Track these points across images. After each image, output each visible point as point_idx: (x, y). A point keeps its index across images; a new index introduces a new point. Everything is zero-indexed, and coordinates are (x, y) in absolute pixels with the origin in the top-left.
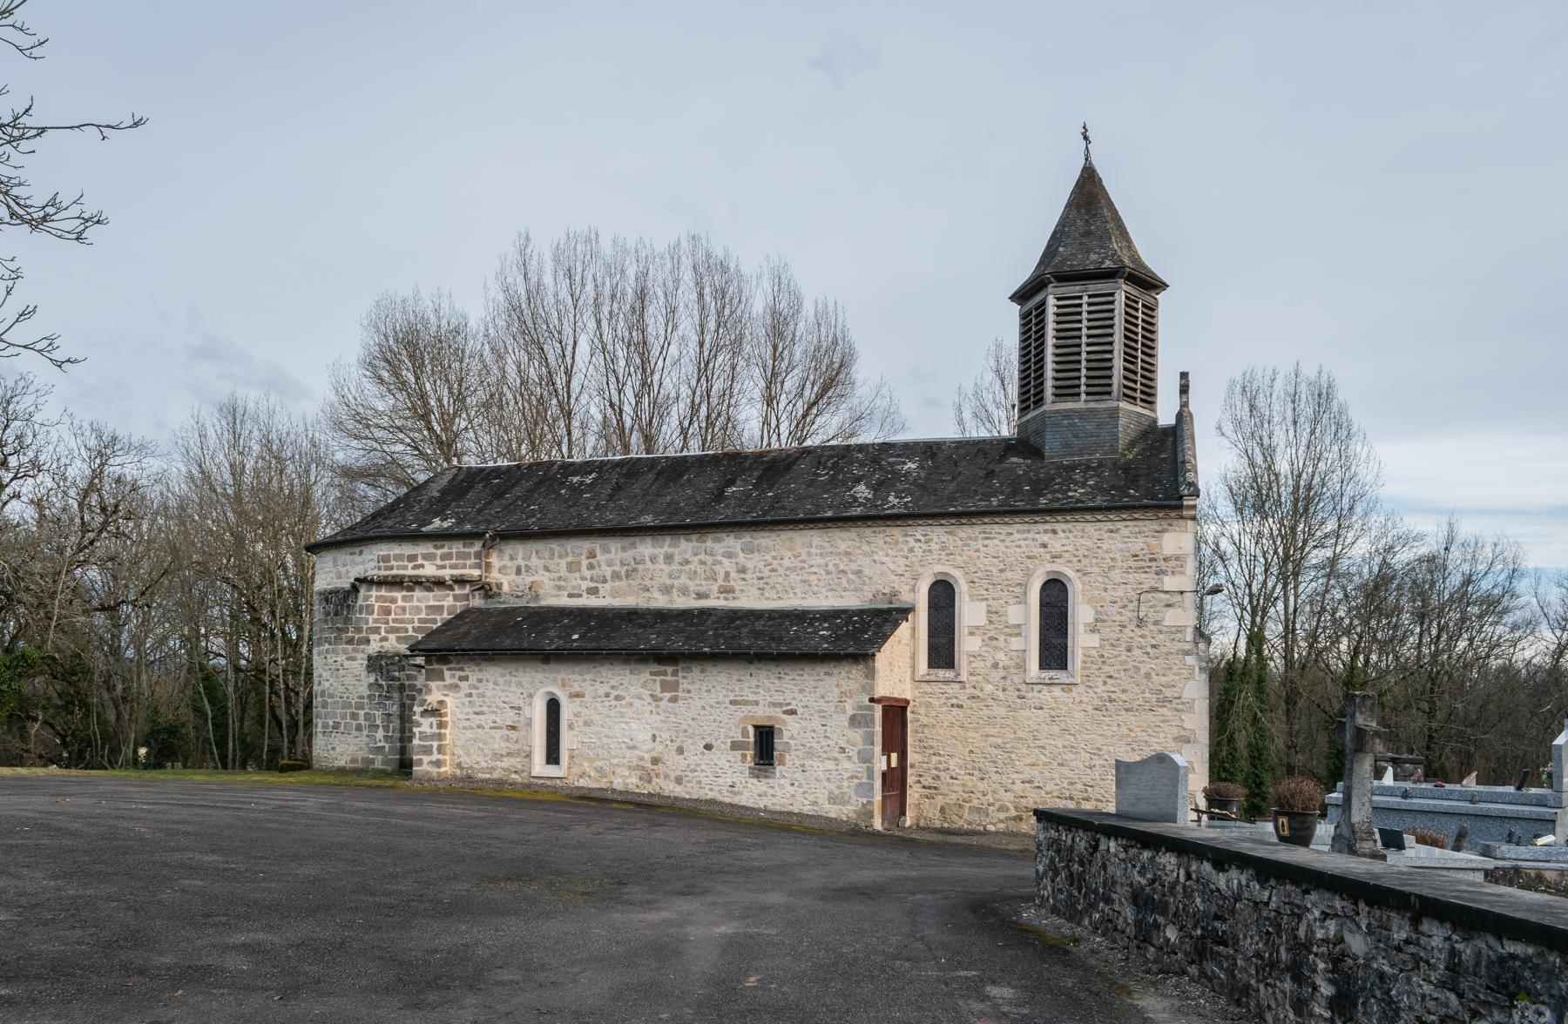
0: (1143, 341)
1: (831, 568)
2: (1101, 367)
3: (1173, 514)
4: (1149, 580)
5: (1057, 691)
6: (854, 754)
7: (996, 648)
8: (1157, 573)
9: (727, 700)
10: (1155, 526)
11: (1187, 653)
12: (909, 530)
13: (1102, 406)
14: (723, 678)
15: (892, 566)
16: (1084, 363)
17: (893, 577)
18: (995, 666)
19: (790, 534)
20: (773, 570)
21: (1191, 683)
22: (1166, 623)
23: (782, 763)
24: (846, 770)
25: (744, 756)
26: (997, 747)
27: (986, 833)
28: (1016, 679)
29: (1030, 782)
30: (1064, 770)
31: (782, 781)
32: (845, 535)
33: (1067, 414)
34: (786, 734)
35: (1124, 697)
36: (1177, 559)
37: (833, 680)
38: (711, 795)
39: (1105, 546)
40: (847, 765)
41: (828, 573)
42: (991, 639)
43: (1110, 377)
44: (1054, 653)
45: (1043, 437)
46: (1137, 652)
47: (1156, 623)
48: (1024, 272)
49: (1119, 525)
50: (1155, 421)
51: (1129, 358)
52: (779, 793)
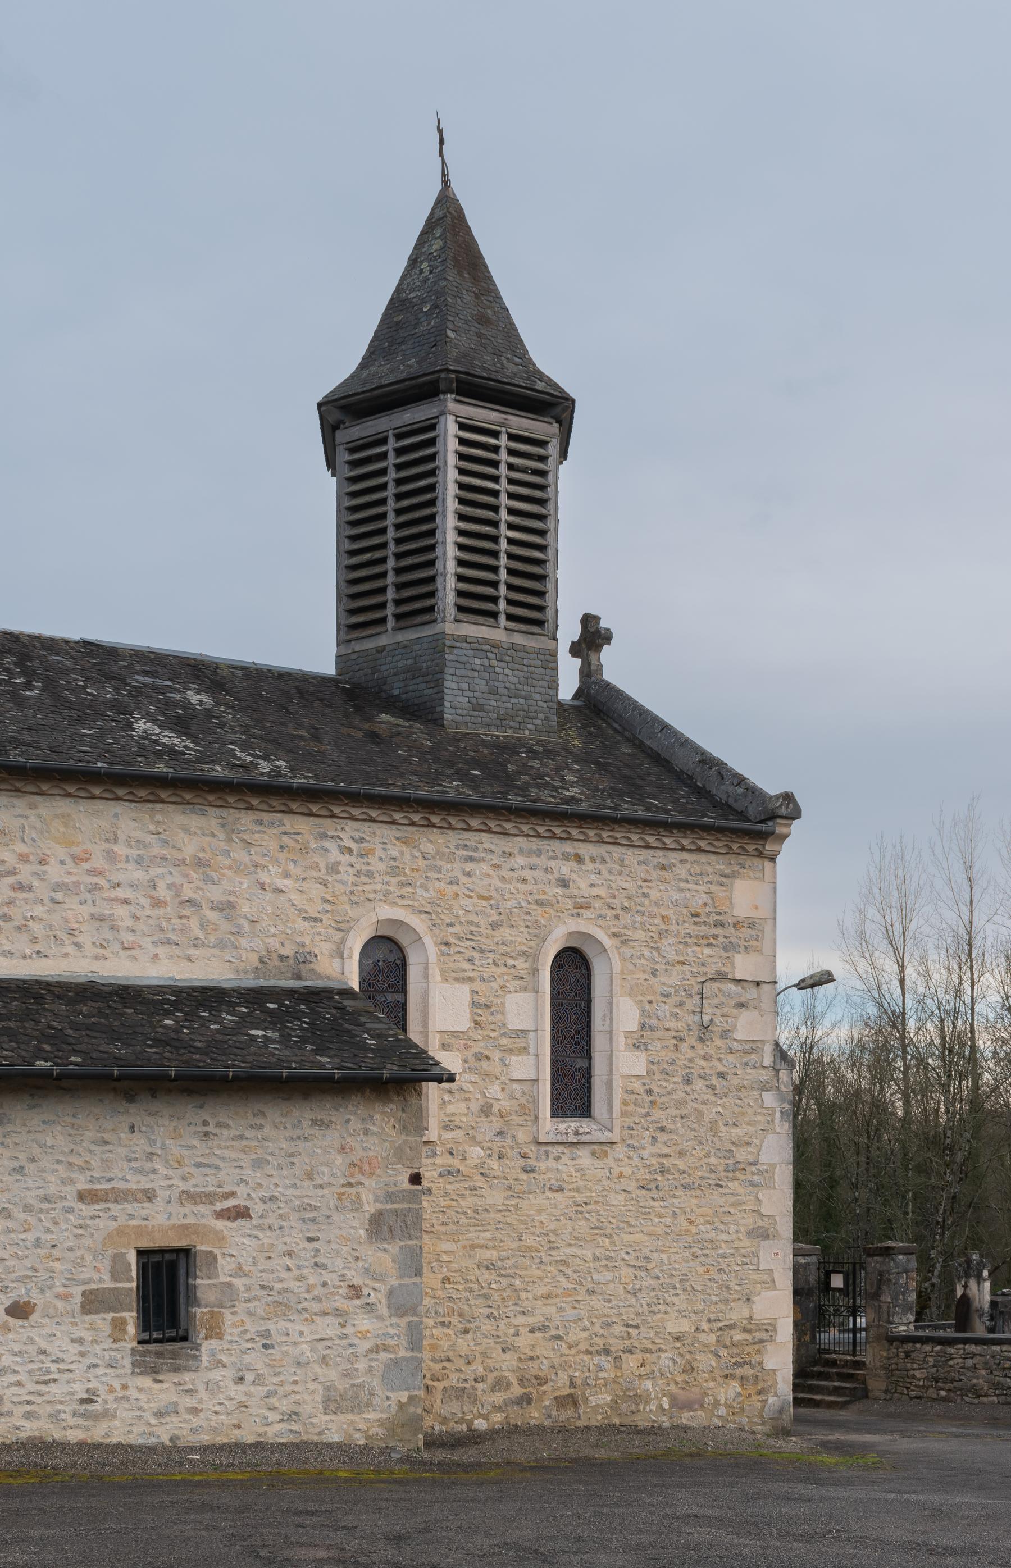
1: (163, 892)
4: (713, 959)
6: (379, 1299)
8: (726, 949)
9: (70, 1191)
10: (719, 864)
11: (764, 1088)
12: (329, 825)
14: (57, 1137)
17: (302, 925)
18: (486, 1110)
19: (63, 806)
20: (20, 887)
23: (215, 1332)
24: (364, 1336)
25: (119, 1326)
27: (475, 1438)
28: (522, 1136)
29: (543, 1329)
30: (597, 1302)
31: (216, 1375)
32: (194, 821)
33: (479, 646)
34: (225, 1265)
36: (752, 925)
37: (331, 1138)
38: (29, 1429)
39: (654, 894)
40: (365, 1323)
41: (157, 903)
44: (573, 1089)
45: (438, 685)
46: (699, 1085)
47: (725, 1034)
48: (340, 356)
52: (209, 1404)
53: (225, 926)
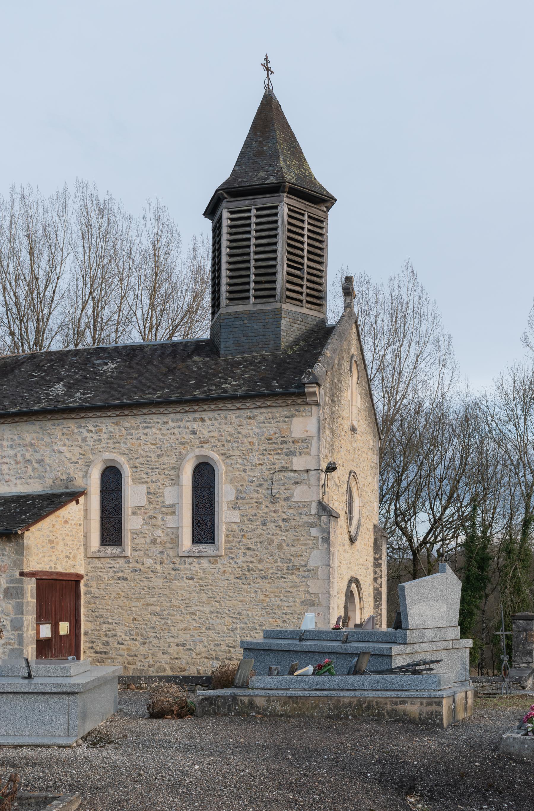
0: (313, 249)
2: (267, 272)
3: (299, 401)
4: (281, 461)
5: (205, 563)
7: (154, 526)
8: (287, 455)
10: (285, 412)
11: (312, 525)
12: (83, 422)
13: (267, 307)
15: (68, 455)
16: (253, 270)
17: (70, 465)
18: (154, 542)
21: (315, 553)
22: (295, 499)
26: (155, 614)
28: (171, 553)
29: (183, 645)
33: (238, 316)
35: (260, 566)
36: (304, 441)
39: (244, 432)
41: (17, 463)
42: (151, 517)
43: (274, 282)
44: (204, 529)
46: (271, 526)
47: (286, 499)
49: (256, 412)
50: (324, 321)
51: (294, 264)
53: (41, 469)
